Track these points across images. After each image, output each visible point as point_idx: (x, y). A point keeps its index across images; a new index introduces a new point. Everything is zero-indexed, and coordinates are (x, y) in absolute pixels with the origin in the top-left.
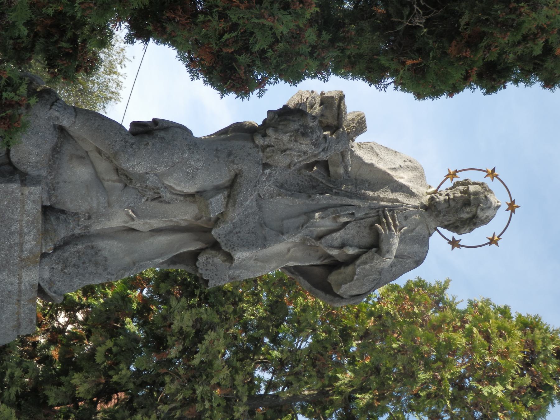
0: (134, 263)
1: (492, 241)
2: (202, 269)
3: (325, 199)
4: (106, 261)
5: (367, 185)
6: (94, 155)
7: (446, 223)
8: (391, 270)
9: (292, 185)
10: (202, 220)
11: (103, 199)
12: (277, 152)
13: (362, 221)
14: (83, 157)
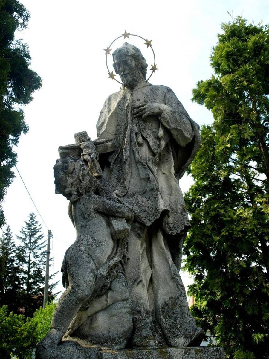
0: (173, 278)
1: (149, 44)
2: (178, 231)
3: (127, 154)
4: (172, 298)
5: (119, 127)
6: (90, 312)
7: (141, 75)
8: (174, 106)
9: (119, 175)
10: (140, 233)
11: (120, 305)
12: (81, 185)
13: (141, 127)
14: (92, 318)
